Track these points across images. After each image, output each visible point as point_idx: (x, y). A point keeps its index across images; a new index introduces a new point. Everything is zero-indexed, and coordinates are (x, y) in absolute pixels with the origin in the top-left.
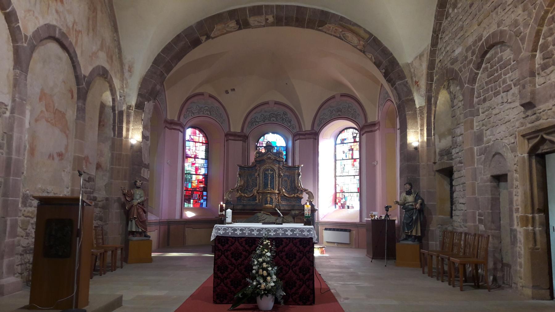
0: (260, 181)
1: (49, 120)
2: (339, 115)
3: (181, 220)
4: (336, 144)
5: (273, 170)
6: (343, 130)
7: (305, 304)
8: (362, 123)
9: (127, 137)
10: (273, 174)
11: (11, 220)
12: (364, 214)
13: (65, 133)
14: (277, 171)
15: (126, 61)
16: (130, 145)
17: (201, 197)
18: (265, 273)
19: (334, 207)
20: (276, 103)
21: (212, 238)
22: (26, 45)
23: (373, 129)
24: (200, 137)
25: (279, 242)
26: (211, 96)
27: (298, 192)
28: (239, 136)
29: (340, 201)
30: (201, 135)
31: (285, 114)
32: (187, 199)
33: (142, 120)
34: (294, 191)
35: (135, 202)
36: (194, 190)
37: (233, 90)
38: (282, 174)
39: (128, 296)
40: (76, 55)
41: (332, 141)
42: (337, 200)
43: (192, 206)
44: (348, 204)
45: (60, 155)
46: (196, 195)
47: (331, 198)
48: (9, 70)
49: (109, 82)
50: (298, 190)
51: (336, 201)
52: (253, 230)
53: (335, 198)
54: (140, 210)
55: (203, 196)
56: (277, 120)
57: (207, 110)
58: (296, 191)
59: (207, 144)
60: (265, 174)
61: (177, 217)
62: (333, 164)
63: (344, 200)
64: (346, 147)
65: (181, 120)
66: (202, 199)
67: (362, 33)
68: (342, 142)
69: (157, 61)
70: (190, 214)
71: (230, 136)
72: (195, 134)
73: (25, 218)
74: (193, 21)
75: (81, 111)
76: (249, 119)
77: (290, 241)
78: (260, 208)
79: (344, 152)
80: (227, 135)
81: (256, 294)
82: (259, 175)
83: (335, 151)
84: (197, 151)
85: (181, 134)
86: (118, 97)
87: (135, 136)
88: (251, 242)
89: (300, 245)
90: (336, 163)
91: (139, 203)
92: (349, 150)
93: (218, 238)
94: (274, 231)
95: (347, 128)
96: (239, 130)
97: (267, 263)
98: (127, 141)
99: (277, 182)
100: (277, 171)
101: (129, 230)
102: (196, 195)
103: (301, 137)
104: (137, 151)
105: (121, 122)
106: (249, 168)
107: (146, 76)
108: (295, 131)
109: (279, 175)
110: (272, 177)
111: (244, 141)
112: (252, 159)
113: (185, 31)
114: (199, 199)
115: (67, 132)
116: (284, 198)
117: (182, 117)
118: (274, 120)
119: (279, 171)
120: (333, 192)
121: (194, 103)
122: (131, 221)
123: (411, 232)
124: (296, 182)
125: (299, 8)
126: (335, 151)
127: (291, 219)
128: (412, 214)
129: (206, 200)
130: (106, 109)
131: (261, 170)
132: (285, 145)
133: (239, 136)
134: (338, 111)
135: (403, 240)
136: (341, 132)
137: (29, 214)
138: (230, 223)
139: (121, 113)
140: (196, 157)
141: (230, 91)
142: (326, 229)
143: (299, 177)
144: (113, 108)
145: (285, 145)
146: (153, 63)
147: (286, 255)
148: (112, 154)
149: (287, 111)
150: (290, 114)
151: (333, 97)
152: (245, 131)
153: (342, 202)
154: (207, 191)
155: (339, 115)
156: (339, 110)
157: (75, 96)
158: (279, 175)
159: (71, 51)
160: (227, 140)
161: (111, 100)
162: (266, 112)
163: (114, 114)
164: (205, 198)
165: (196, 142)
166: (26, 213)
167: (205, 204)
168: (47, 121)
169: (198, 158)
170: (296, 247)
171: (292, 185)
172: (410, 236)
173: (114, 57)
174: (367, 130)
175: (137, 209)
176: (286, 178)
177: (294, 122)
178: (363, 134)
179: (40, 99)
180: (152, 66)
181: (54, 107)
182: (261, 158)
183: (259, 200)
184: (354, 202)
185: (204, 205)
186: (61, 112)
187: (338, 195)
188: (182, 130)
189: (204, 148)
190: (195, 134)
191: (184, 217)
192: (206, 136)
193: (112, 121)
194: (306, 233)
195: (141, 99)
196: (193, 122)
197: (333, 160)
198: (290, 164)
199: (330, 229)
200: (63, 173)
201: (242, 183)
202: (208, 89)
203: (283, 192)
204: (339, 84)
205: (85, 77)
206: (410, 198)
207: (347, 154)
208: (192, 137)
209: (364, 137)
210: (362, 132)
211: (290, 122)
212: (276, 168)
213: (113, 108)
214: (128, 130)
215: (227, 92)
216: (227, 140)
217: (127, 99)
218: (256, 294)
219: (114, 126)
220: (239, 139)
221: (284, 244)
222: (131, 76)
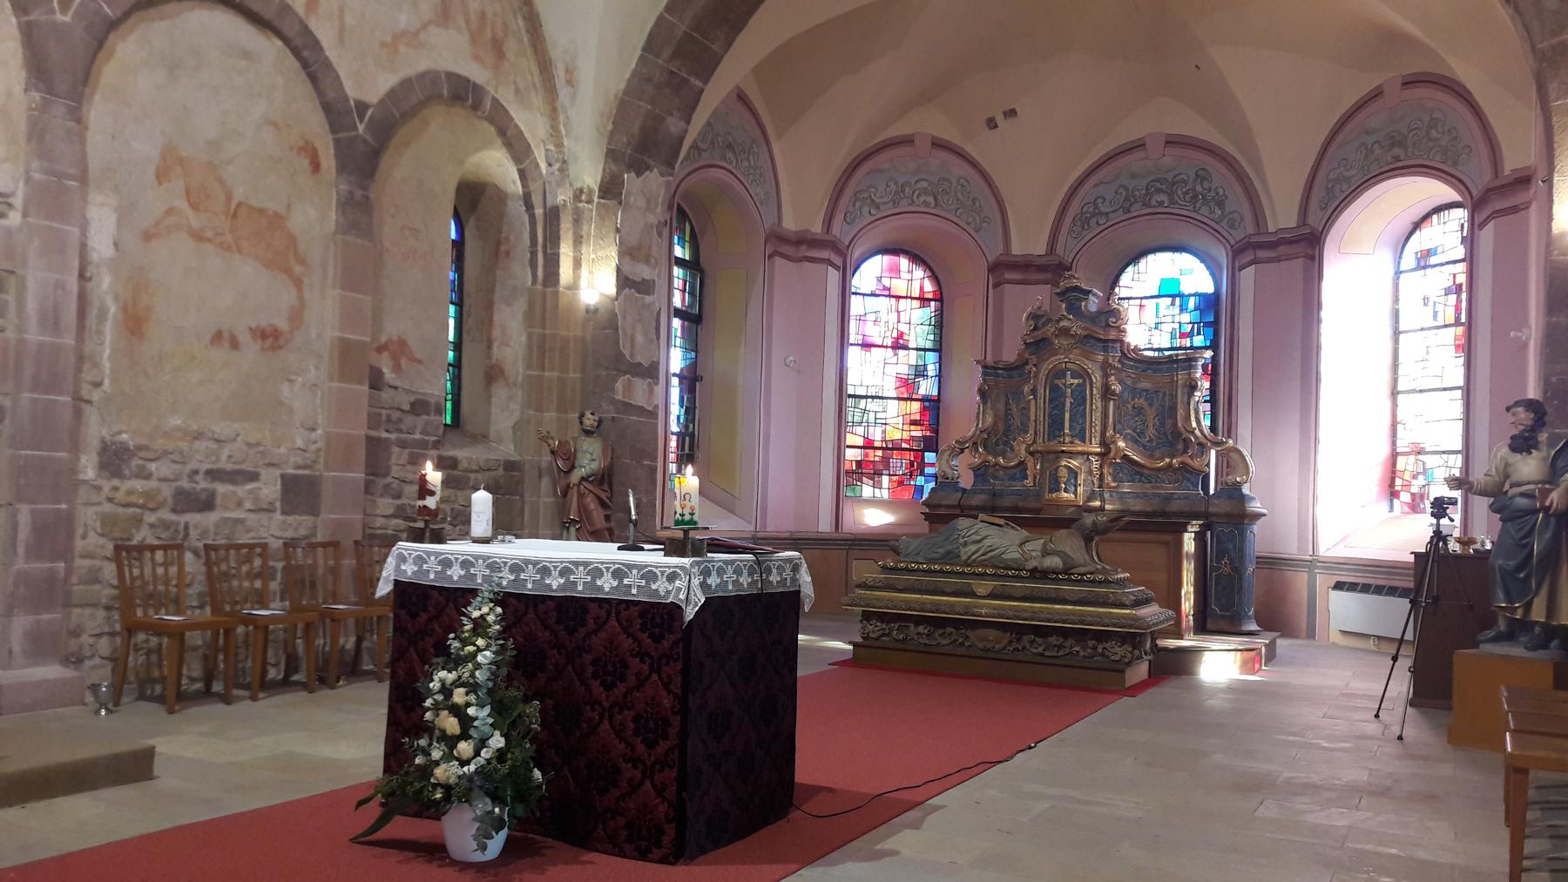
0: (1038, 410)
1: (209, 234)
2: (1397, 159)
3: (835, 536)
4: (1398, 273)
5: (1083, 374)
6: (1427, 217)
7: (643, 855)
8: (1481, 178)
9: (574, 286)
10: (1081, 386)
11: (33, 513)
13: (287, 271)
14: (1097, 378)
15: (555, 54)
16: (582, 307)
18: (451, 724)
19: (1385, 505)
20: (1172, 141)
21: (384, 589)
22: (67, 18)
23: (1518, 199)
26: (938, 144)
27: (1185, 452)
28: (1041, 268)
29: (1407, 486)
30: (919, 273)
31: (1202, 175)
33: (618, 230)
34: (1171, 445)
37: (1011, 113)
38: (1117, 388)
39: (165, 747)
40: (317, 43)
41: (1385, 258)
42: (1398, 482)
43: (885, 494)
45: (270, 337)
46: (899, 464)
47: (1374, 474)
48: (9, 94)
49: (491, 120)
50: (1186, 442)
51: (1392, 484)
52: (545, 571)
53: (1392, 472)
55: (922, 465)
56: (1172, 202)
57: (925, 192)
58: (1180, 446)
60: (1055, 389)
61: (825, 526)
62: (1389, 346)
63: (1421, 480)
65: (836, 230)
66: (922, 474)
68: (1424, 260)
70: (876, 518)
71: (1005, 269)
72: (895, 271)
73: (120, 510)
75: (358, 211)
77: (609, 614)
79: (1426, 301)
80: (994, 268)
82: (1034, 391)
83: (1396, 300)
86: (543, 166)
87: (592, 278)
89: (643, 630)
90: (1396, 342)
91: (583, 479)
92: (1448, 292)
93: (402, 588)
94: (561, 574)
95: (1438, 210)
96: (1039, 248)
97: (472, 687)
98: (575, 298)
99: (1097, 416)
100: (1097, 378)
103: (1262, 254)
104: (606, 323)
105: (553, 239)
106: (1009, 368)
107: (625, 92)
108: (1239, 235)
109: (1107, 393)
110: (1080, 399)
115: (297, 269)
117: (838, 220)
118: (1161, 204)
119: (1106, 376)
120: (1385, 451)
121: (879, 171)
123: (1528, 607)
124: (1180, 413)
126: (1396, 300)
128: (1530, 533)
130: (509, 203)
131: (1042, 376)
132: (1210, 289)
133: (1041, 268)
134: (1392, 145)
135: (1496, 639)
136: (1417, 226)
137: (133, 499)
138: (486, 541)
141: (1000, 119)
142: (1339, 586)
143: (1191, 394)
144: (527, 199)
146: (644, 49)
147: (595, 662)
148: (530, 336)
150: (1221, 177)
151: (1376, 94)
152: (1060, 250)
153: (1414, 490)
155: (1397, 159)
156: (1397, 141)
157: (329, 162)
158: (1107, 393)
159: (291, 31)
160: (996, 286)
161: (516, 176)
162: (1133, 176)
163: (532, 217)
165: (898, 297)
166: (120, 496)
168: (198, 236)
170: (629, 635)
171: (1162, 424)
172: (1525, 625)
173: (511, 46)
174: (1498, 205)
175: (581, 496)
176: (1142, 402)
177: (1237, 201)
178: (1242, 268)
179: (162, 175)
180: (642, 58)
181: (229, 197)
186: (262, 211)
187: (1401, 463)
188: (838, 261)
190: (895, 271)
193: (527, 242)
194: (661, 586)
195: (614, 168)
196: (885, 231)
197: (1389, 332)
199: (1352, 587)
200: (285, 390)
201: (990, 420)
202: (931, 123)
203: (1118, 449)
204: (1393, 40)
205: (362, 107)
206: (1529, 467)
207: (1439, 308)
208: (886, 282)
210: (1479, 219)
211: (1221, 204)
212: (1090, 367)
213: (527, 199)
214: (577, 264)
215: (992, 124)
216: (996, 286)
217: (572, 170)
219: (534, 254)
220: (1041, 276)
221: (591, 624)
222: (574, 96)
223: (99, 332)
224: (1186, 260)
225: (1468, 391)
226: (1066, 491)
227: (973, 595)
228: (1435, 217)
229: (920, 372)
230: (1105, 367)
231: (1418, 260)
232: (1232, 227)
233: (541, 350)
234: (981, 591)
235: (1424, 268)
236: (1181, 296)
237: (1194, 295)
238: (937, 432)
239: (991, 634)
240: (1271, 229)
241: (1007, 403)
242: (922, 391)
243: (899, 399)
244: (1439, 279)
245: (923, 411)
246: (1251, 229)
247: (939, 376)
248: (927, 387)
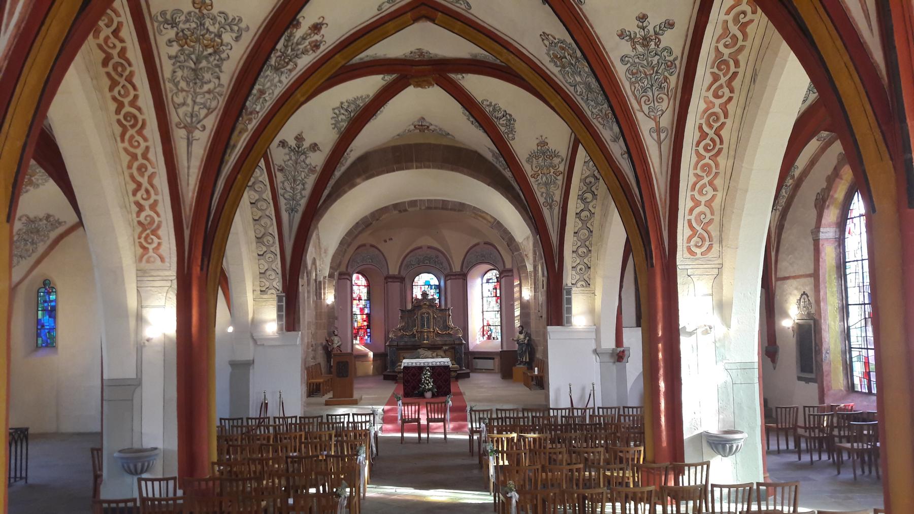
0: (418, 322)
5: (428, 313)
8: (502, 268)
12: (504, 344)
15: (322, 246)
20: (429, 247)
24: (362, 281)
25: (433, 368)
26: (372, 246)
31: (437, 257)
32: (355, 336)
35: (335, 346)
36: (360, 328)
44: (493, 335)
59: (368, 286)
67: (489, 218)
68: (488, 282)
69: (342, 243)
71: (389, 278)
74: (367, 213)
76: (405, 262)
80: (386, 278)
81: (425, 390)
85: (349, 282)
88: (421, 369)
102: (361, 332)
104: (331, 308)
105: (320, 289)
108: (446, 272)
110: (428, 319)
111: (402, 282)
112: (409, 307)
113: (361, 220)
116: (438, 334)
125: (443, 201)
127: (442, 354)
129: (370, 336)
139: (320, 282)
140: (360, 299)
149: (440, 255)
151: (477, 244)
177: (445, 264)
184: (496, 333)
189: (365, 290)
191: (277, 336)
192: (367, 280)
198: (443, 307)
206: (522, 336)
215: (385, 241)
218: (425, 390)
223: (437, 356)
224: (431, 276)
229: (365, 306)
230: (433, 312)
233: (318, 315)
244: (491, 286)
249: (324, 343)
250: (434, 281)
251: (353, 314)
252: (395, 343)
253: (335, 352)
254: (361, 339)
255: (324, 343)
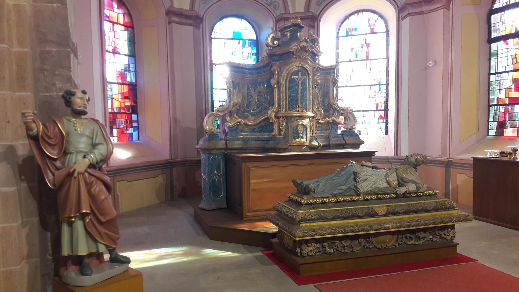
14: (311, 75)
17: (129, 122)
28: (187, 17)
46: (121, 121)
54: (98, 188)
55: (131, 122)
58: (331, 112)
64: (356, 42)
66: (132, 127)
68: (350, 34)
78: (285, 147)
82: (278, 83)
84: (116, 40)
91: (92, 166)
101: (66, 251)
102: (121, 121)
108: (278, 13)
114: (127, 128)
122: (71, 224)
129: (137, 128)
131: (284, 74)
132: (255, 38)
133: (187, 17)
140: (115, 52)
145: (255, 38)
154: (137, 114)
160: (170, 23)
164: (135, 125)
165: (113, 23)
167: (135, 134)
169: (119, 53)
171: (323, 101)
174: (411, 11)
175: (89, 185)
178: (403, 19)
182: (285, 49)
183: (280, 131)
185: (135, 138)
192: (128, 14)
207: (358, 52)
209: (406, 23)
210: (402, 15)
216: (170, 23)
225: (212, 89)
226: (302, 138)
227: (376, 215)
228: (356, 14)
229: (127, 69)
231: (348, 33)
232: (275, 9)
234: (381, 212)
235: (351, 35)
236: (242, 40)
237: (249, 40)
238: (136, 102)
239: (387, 238)
240: (291, 12)
241: (248, 89)
242: (128, 80)
243: (118, 83)
245: (130, 90)
246: (283, 11)
247: (136, 71)
248: (130, 78)
249: (23, 148)
250: (250, 33)
251: (104, 83)
252: (221, 144)
253: (78, 191)
254: (121, 133)
255: (23, 148)
